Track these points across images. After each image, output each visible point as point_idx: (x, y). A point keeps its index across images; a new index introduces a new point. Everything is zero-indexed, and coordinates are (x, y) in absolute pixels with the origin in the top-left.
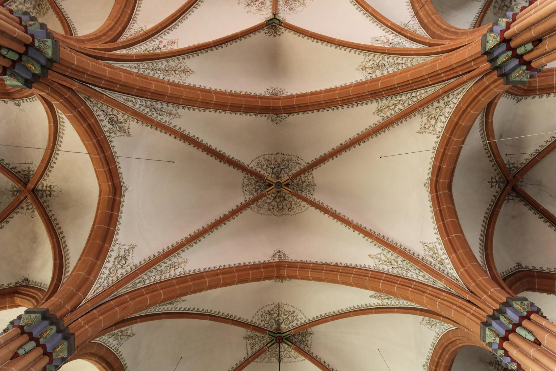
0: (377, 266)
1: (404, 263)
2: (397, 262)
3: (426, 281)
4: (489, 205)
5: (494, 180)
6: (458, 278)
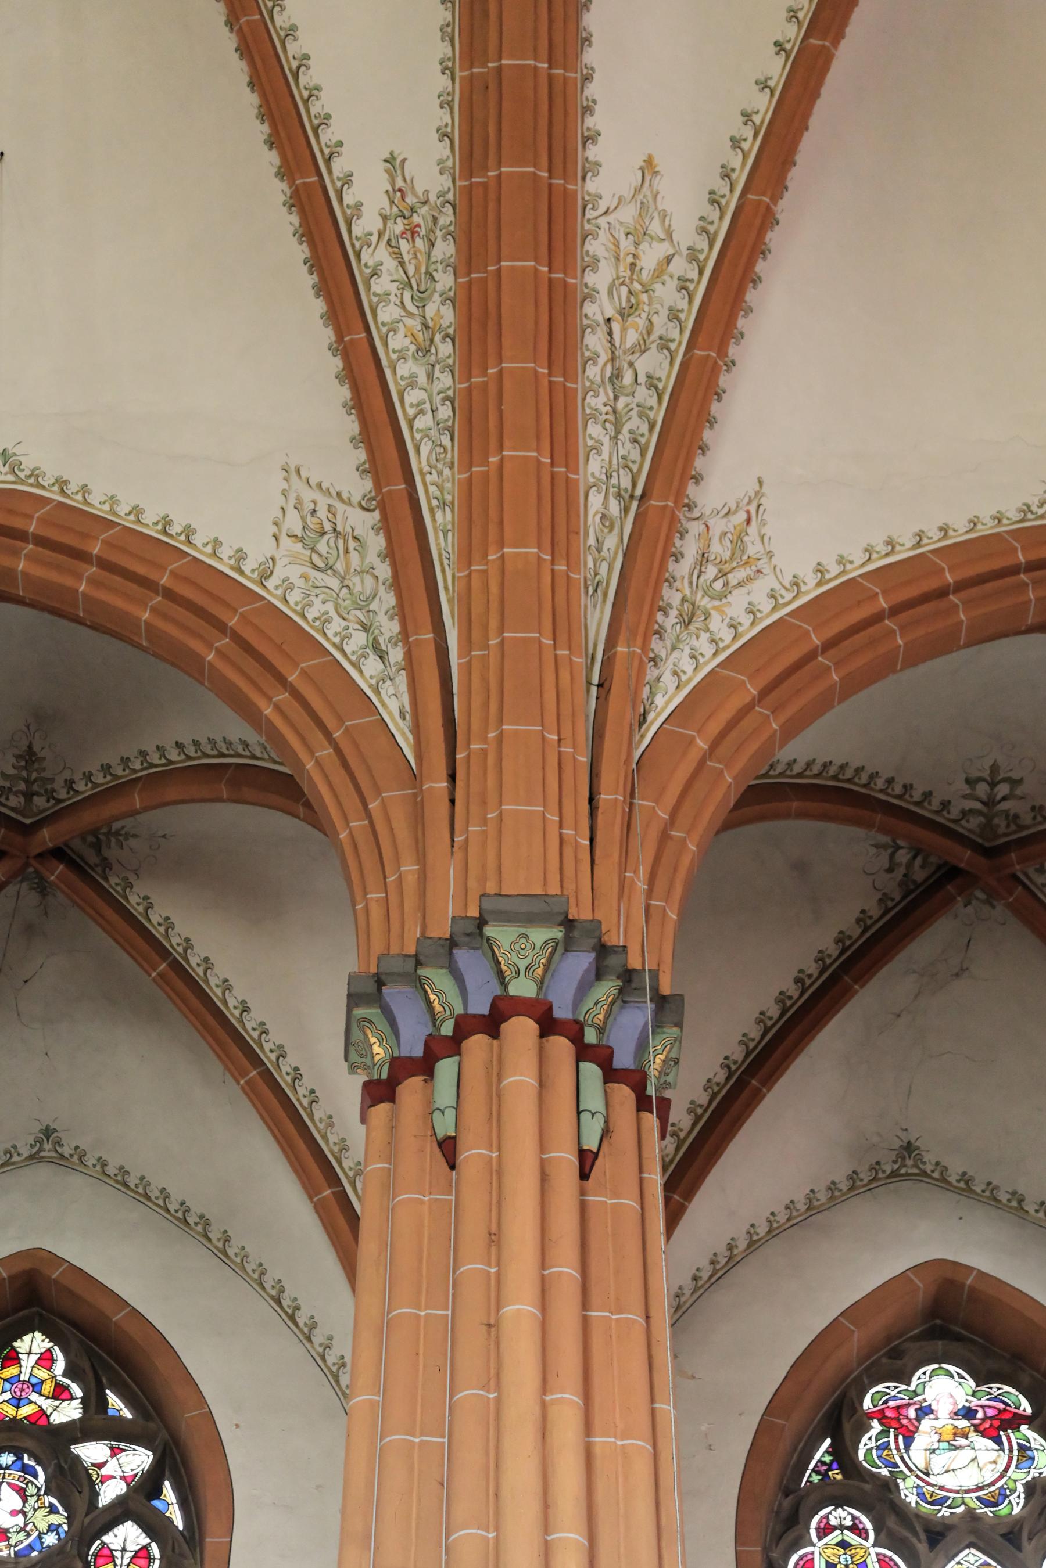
0: (602, 221)
1: (643, 394)
2: (641, 348)
3: (591, 541)
4: (890, 775)
5: (1003, 789)
6: (655, 722)
